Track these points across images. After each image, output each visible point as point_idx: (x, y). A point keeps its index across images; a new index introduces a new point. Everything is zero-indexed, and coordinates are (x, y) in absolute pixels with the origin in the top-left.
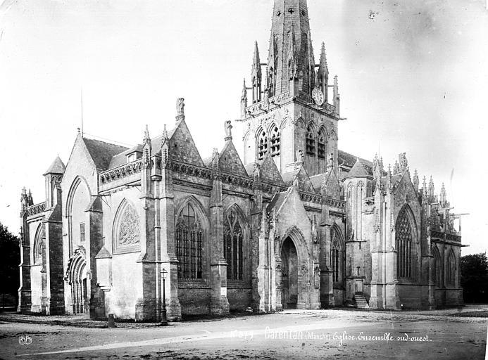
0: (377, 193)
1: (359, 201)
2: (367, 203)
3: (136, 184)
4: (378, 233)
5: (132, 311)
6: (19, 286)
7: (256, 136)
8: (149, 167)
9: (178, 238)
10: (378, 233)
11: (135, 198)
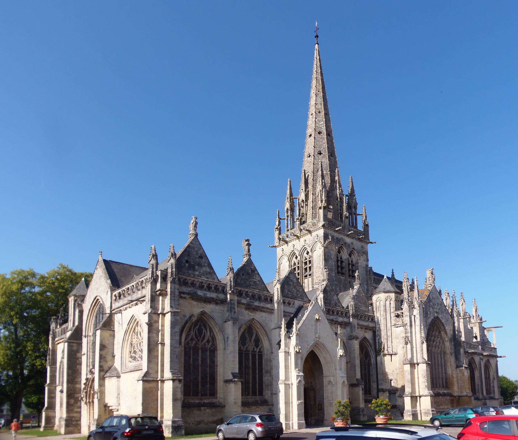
0: (405, 306)
1: (388, 315)
2: (396, 316)
3: (140, 300)
4: (409, 346)
5: (511, 420)
6: (44, 405)
7: (290, 260)
8: (154, 281)
9: (187, 354)
10: (409, 346)
11: (140, 312)
